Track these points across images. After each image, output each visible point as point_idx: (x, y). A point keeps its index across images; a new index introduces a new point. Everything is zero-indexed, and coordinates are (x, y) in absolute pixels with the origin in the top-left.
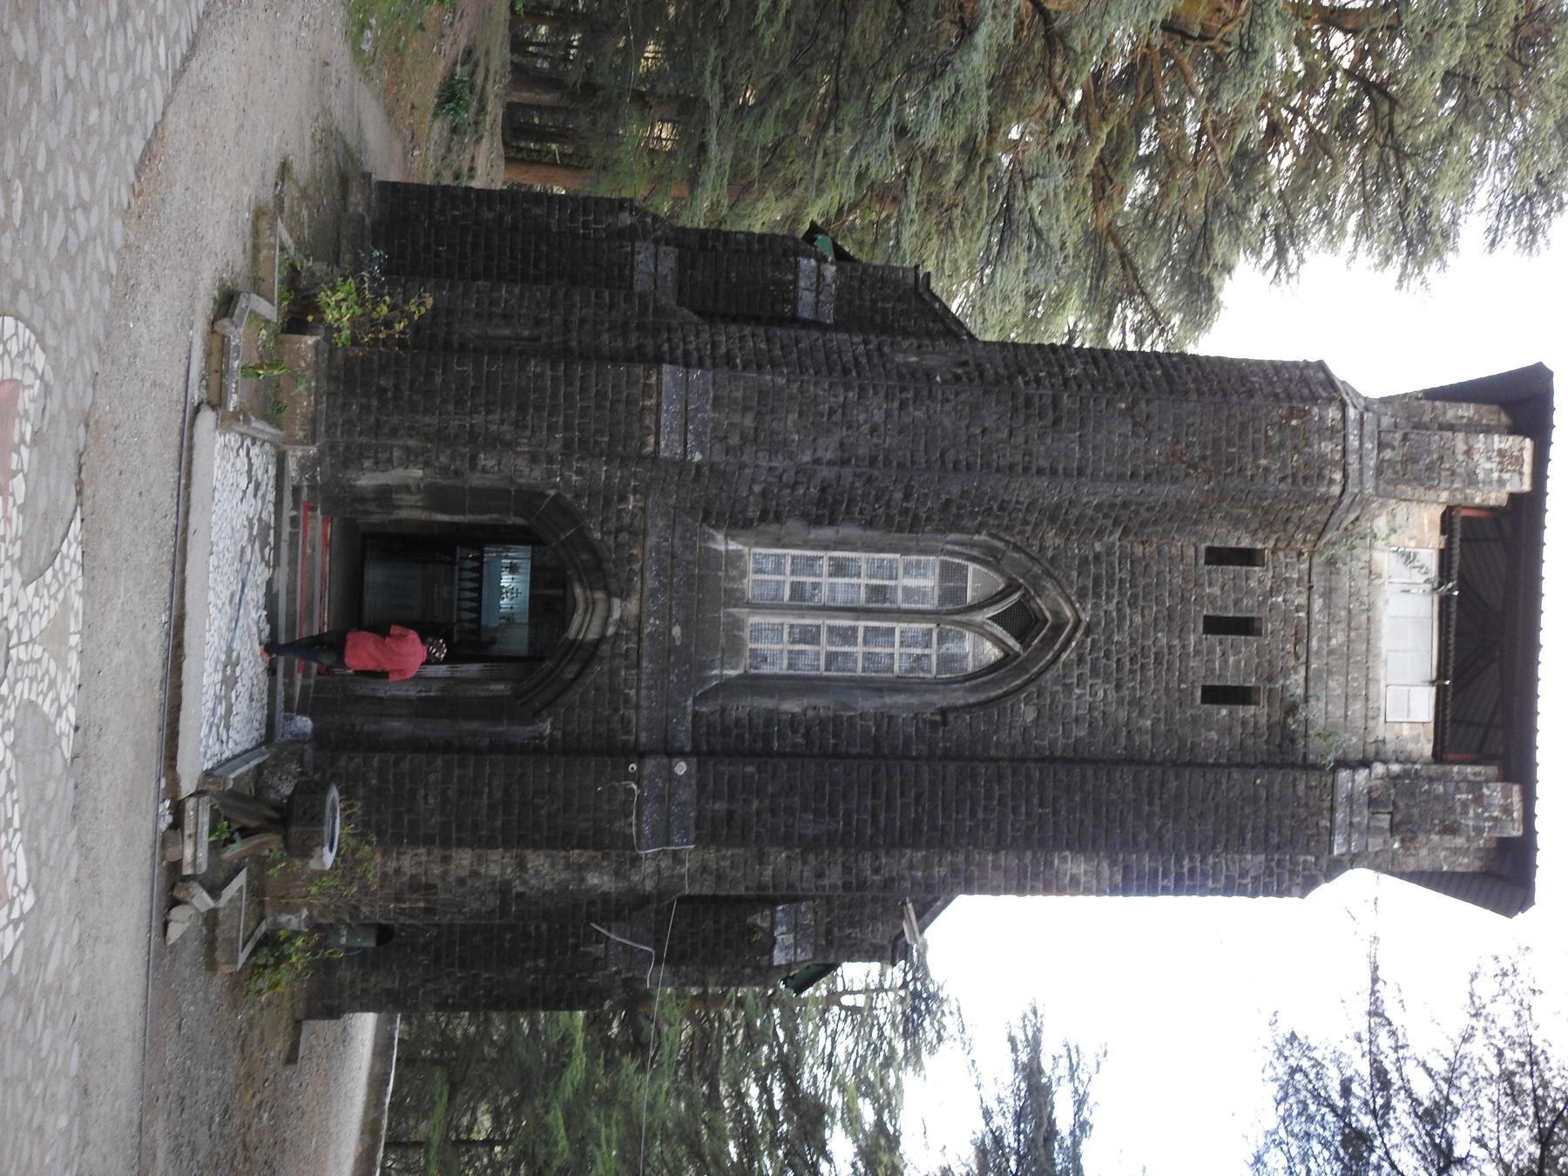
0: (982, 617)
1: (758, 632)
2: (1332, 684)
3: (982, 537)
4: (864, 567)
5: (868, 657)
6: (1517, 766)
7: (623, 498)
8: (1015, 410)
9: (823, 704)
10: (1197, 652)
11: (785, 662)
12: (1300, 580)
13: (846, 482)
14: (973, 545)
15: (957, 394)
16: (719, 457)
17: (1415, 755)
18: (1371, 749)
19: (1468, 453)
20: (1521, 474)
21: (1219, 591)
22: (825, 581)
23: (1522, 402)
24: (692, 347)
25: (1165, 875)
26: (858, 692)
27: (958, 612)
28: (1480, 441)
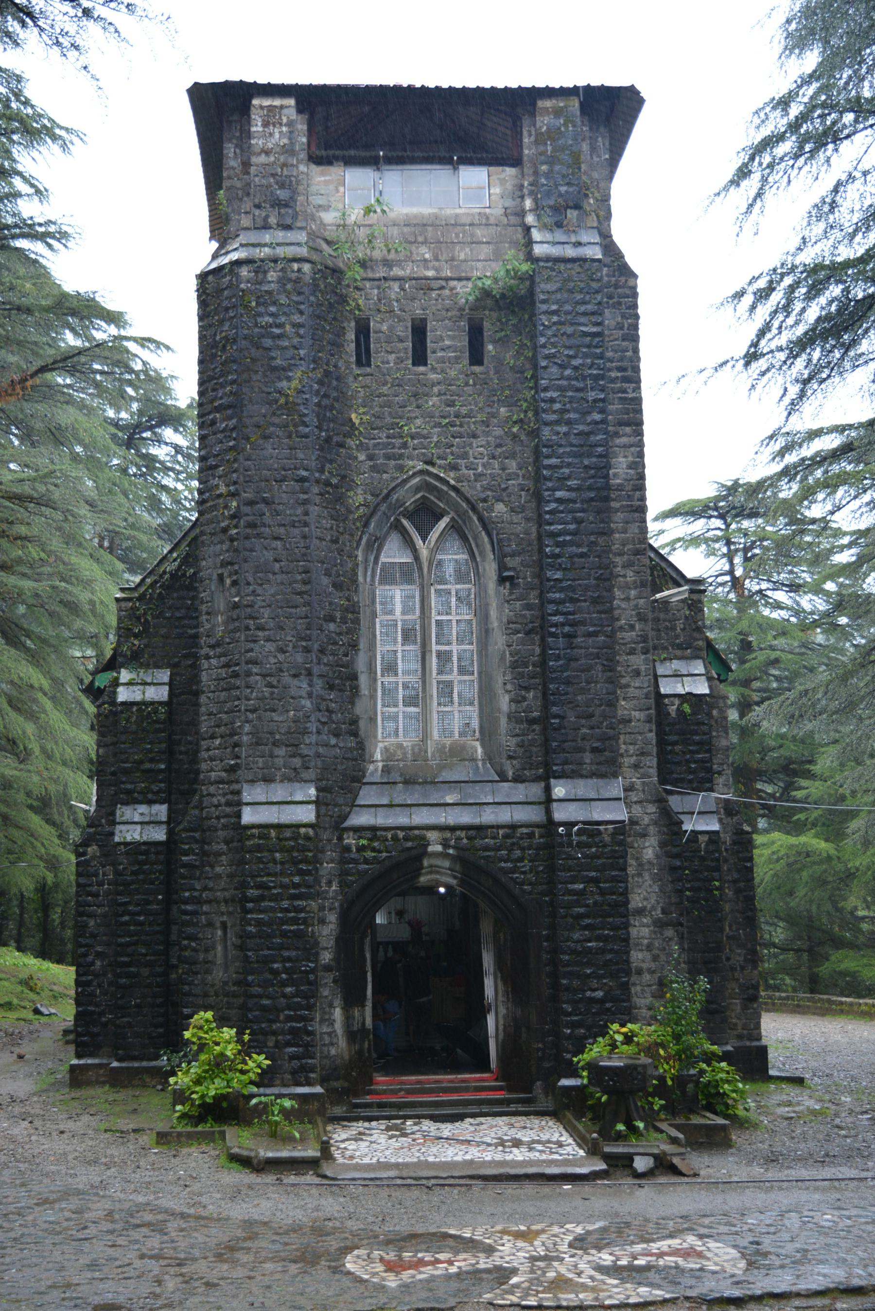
0: (424, 553)
1: (445, 732)
2: (462, 256)
3: (360, 554)
4: (389, 648)
5: (460, 641)
6: (519, 102)
7: (347, 849)
8: (259, 536)
9: (500, 678)
10: (443, 371)
11: (468, 708)
12: (378, 288)
13: (324, 669)
14: (366, 561)
15: (248, 584)
16: (311, 774)
17: (516, 182)
18: (513, 220)
19: (267, 153)
20: (282, 107)
21: (392, 357)
22: (401, 679)
23: (221, 109)
24: (223, 800)
25: (625, 391)
26: (490, 649)
27: (420, 569)
28: (257, 142)
